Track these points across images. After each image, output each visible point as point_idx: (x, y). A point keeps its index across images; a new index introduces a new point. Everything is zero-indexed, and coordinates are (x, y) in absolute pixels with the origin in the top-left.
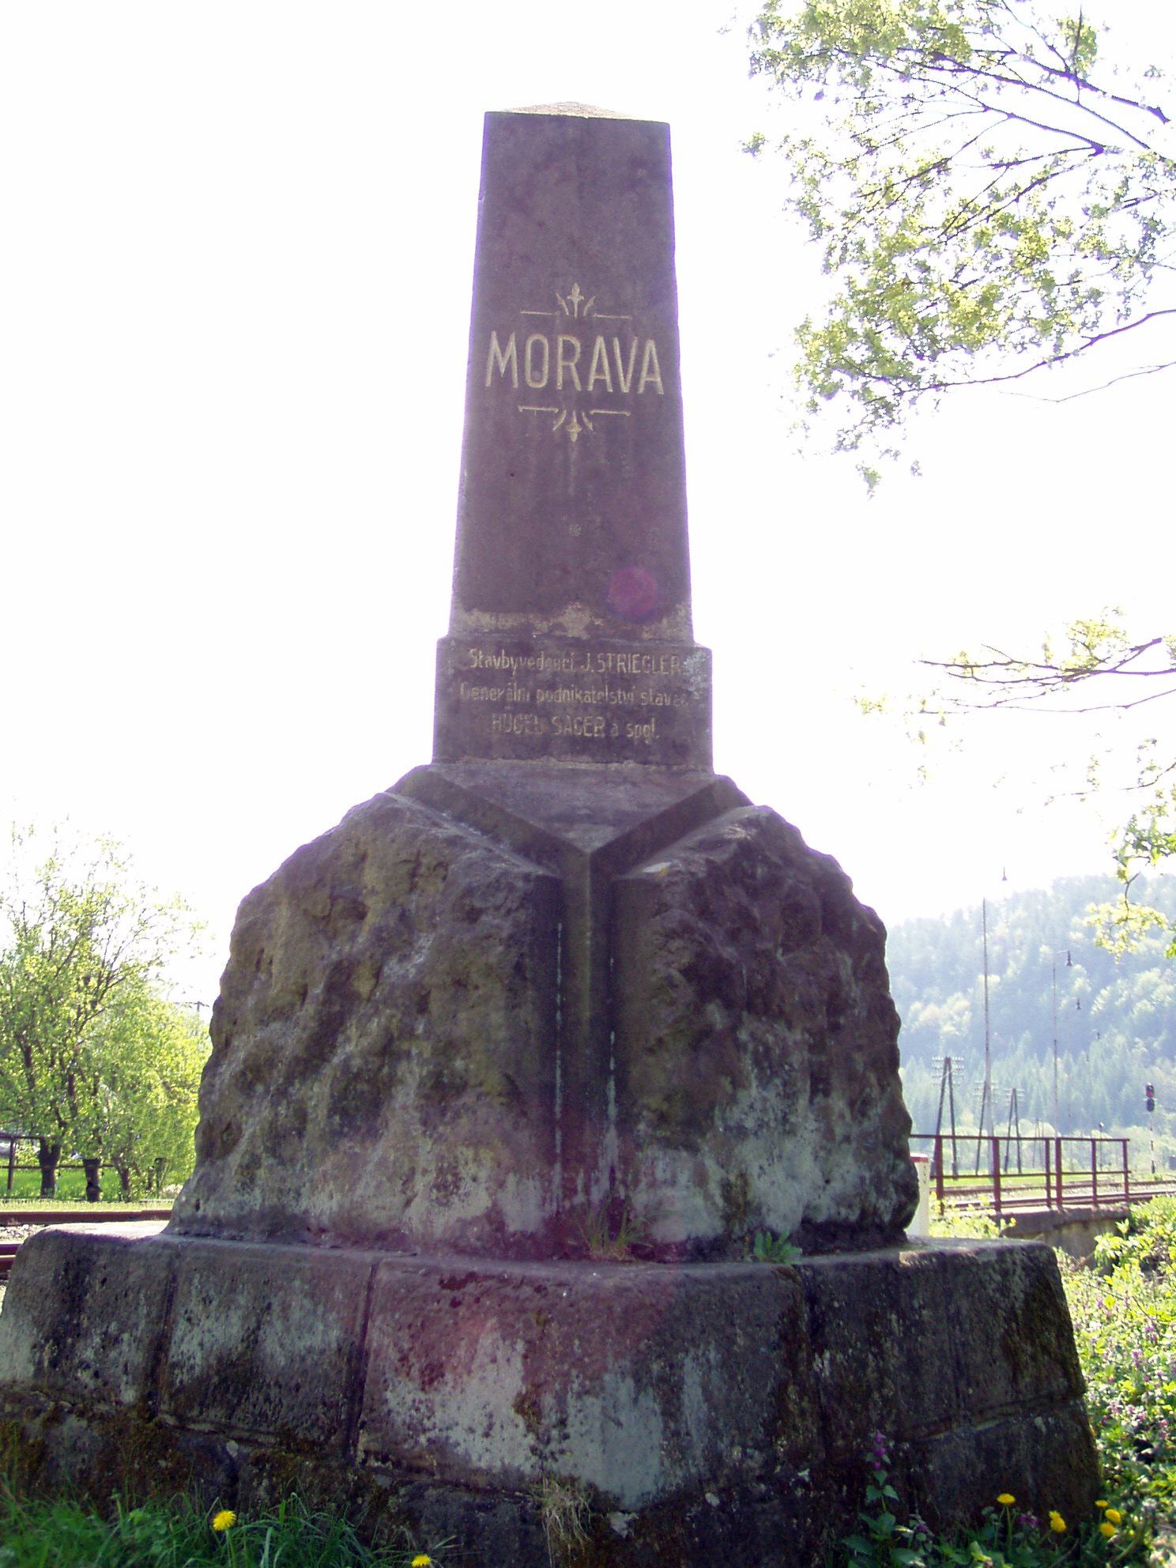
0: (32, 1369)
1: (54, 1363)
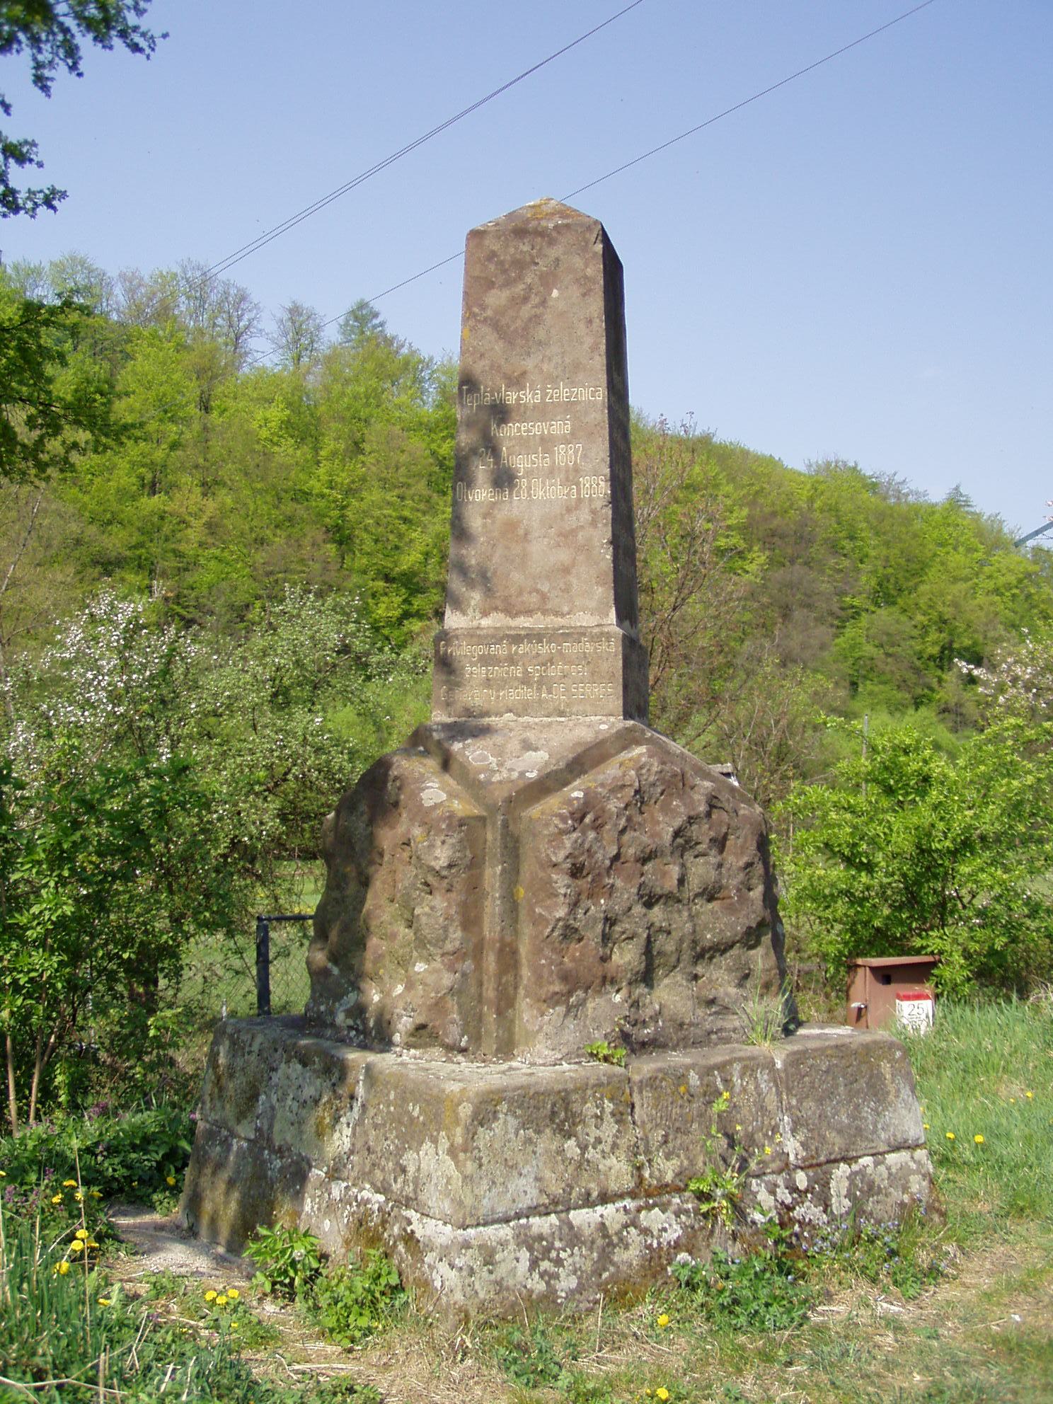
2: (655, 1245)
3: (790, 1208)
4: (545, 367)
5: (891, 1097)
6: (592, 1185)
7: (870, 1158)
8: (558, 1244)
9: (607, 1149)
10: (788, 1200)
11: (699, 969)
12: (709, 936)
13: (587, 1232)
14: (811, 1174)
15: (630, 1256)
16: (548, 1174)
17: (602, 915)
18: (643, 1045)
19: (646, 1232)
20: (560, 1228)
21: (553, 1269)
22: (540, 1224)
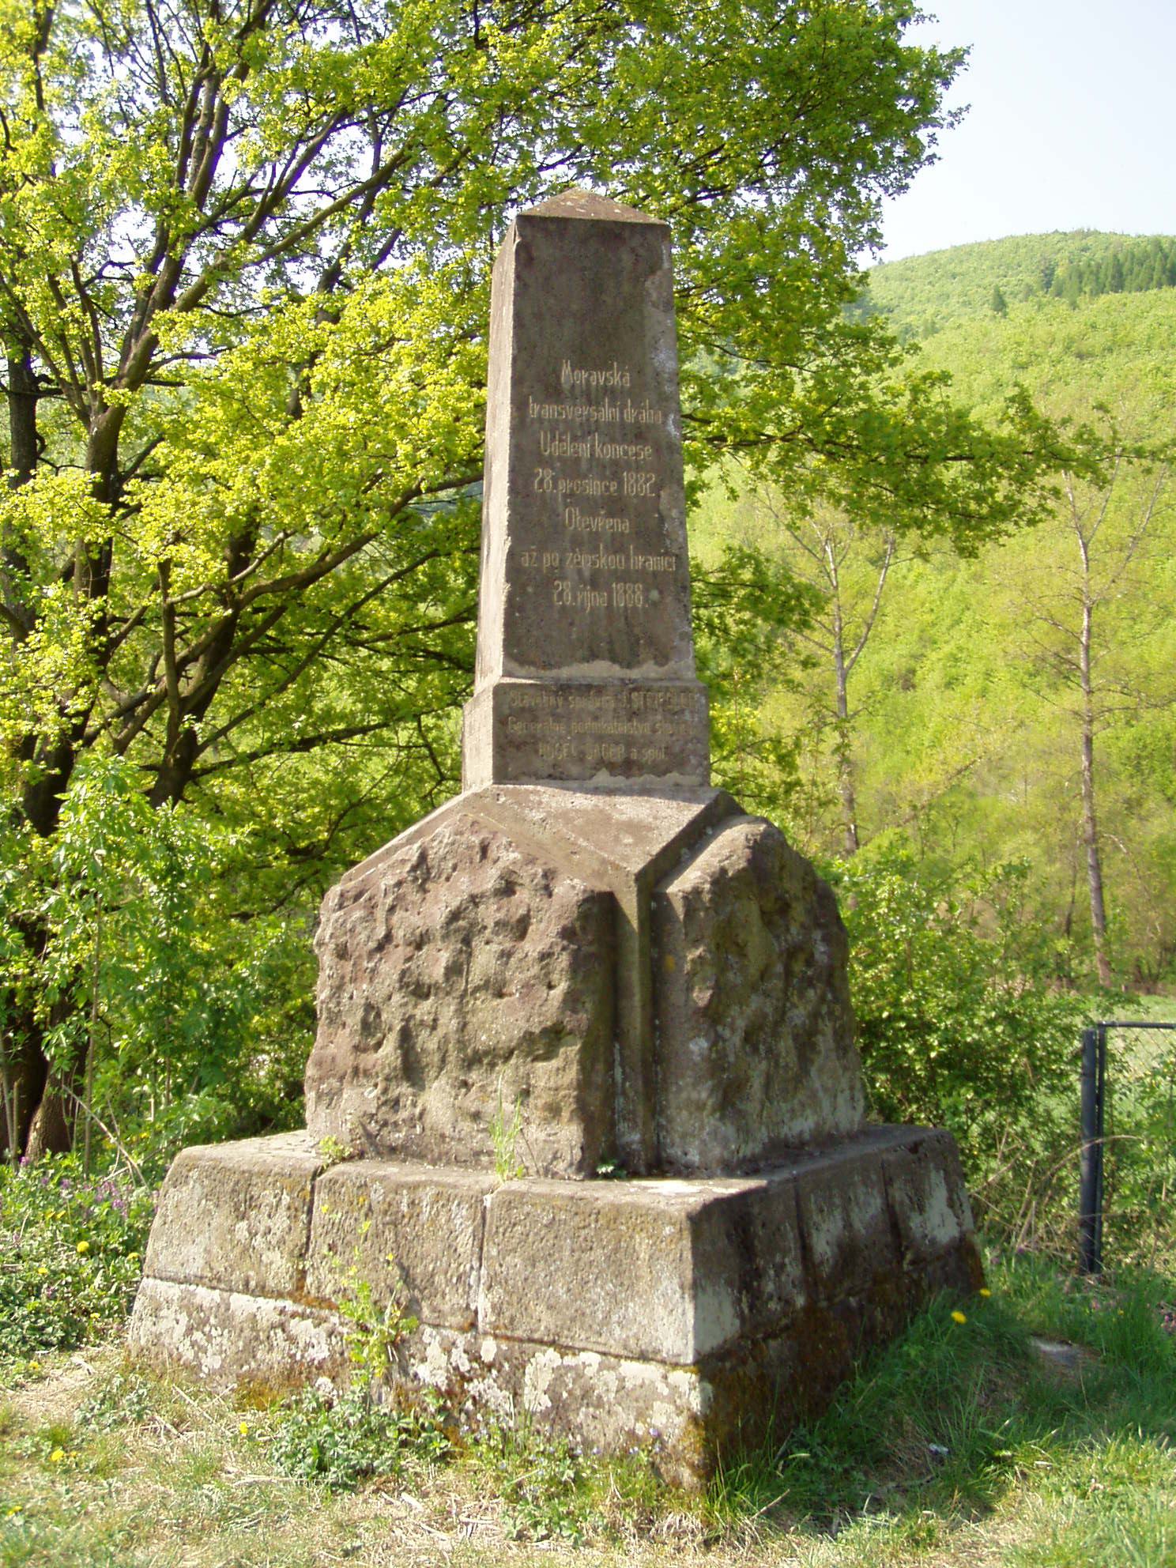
0: (737, 1322)
1: (751, 1307)
2: (298, 1357)
3: (465, 1378)
4: (57, 499)
5: (642, 1286)
6: (252, 1273)
7: (598, 1357)
8: (212, 1321)
9: (274, 1242)
10: (465, 1367)
11: (474, 1076)
12: (484, 1038)
13: (237, 1320)
14: (504, 1347)
15: (273, 1358)
16: (215, 1249)
17: (363, 1001)
18: (393, 1150)
19: (292, 1339)
20: (219, 1306)
21: (203, 1342)
22: (206, 1296)
